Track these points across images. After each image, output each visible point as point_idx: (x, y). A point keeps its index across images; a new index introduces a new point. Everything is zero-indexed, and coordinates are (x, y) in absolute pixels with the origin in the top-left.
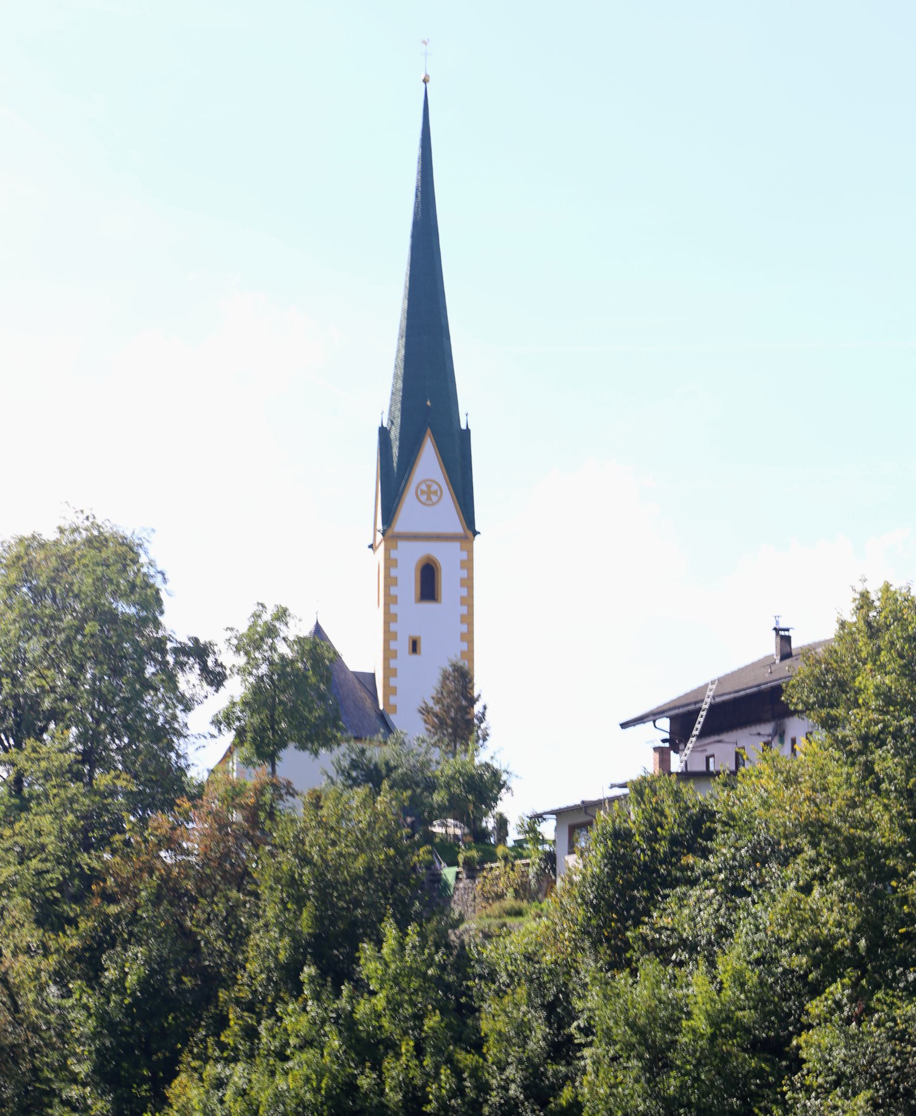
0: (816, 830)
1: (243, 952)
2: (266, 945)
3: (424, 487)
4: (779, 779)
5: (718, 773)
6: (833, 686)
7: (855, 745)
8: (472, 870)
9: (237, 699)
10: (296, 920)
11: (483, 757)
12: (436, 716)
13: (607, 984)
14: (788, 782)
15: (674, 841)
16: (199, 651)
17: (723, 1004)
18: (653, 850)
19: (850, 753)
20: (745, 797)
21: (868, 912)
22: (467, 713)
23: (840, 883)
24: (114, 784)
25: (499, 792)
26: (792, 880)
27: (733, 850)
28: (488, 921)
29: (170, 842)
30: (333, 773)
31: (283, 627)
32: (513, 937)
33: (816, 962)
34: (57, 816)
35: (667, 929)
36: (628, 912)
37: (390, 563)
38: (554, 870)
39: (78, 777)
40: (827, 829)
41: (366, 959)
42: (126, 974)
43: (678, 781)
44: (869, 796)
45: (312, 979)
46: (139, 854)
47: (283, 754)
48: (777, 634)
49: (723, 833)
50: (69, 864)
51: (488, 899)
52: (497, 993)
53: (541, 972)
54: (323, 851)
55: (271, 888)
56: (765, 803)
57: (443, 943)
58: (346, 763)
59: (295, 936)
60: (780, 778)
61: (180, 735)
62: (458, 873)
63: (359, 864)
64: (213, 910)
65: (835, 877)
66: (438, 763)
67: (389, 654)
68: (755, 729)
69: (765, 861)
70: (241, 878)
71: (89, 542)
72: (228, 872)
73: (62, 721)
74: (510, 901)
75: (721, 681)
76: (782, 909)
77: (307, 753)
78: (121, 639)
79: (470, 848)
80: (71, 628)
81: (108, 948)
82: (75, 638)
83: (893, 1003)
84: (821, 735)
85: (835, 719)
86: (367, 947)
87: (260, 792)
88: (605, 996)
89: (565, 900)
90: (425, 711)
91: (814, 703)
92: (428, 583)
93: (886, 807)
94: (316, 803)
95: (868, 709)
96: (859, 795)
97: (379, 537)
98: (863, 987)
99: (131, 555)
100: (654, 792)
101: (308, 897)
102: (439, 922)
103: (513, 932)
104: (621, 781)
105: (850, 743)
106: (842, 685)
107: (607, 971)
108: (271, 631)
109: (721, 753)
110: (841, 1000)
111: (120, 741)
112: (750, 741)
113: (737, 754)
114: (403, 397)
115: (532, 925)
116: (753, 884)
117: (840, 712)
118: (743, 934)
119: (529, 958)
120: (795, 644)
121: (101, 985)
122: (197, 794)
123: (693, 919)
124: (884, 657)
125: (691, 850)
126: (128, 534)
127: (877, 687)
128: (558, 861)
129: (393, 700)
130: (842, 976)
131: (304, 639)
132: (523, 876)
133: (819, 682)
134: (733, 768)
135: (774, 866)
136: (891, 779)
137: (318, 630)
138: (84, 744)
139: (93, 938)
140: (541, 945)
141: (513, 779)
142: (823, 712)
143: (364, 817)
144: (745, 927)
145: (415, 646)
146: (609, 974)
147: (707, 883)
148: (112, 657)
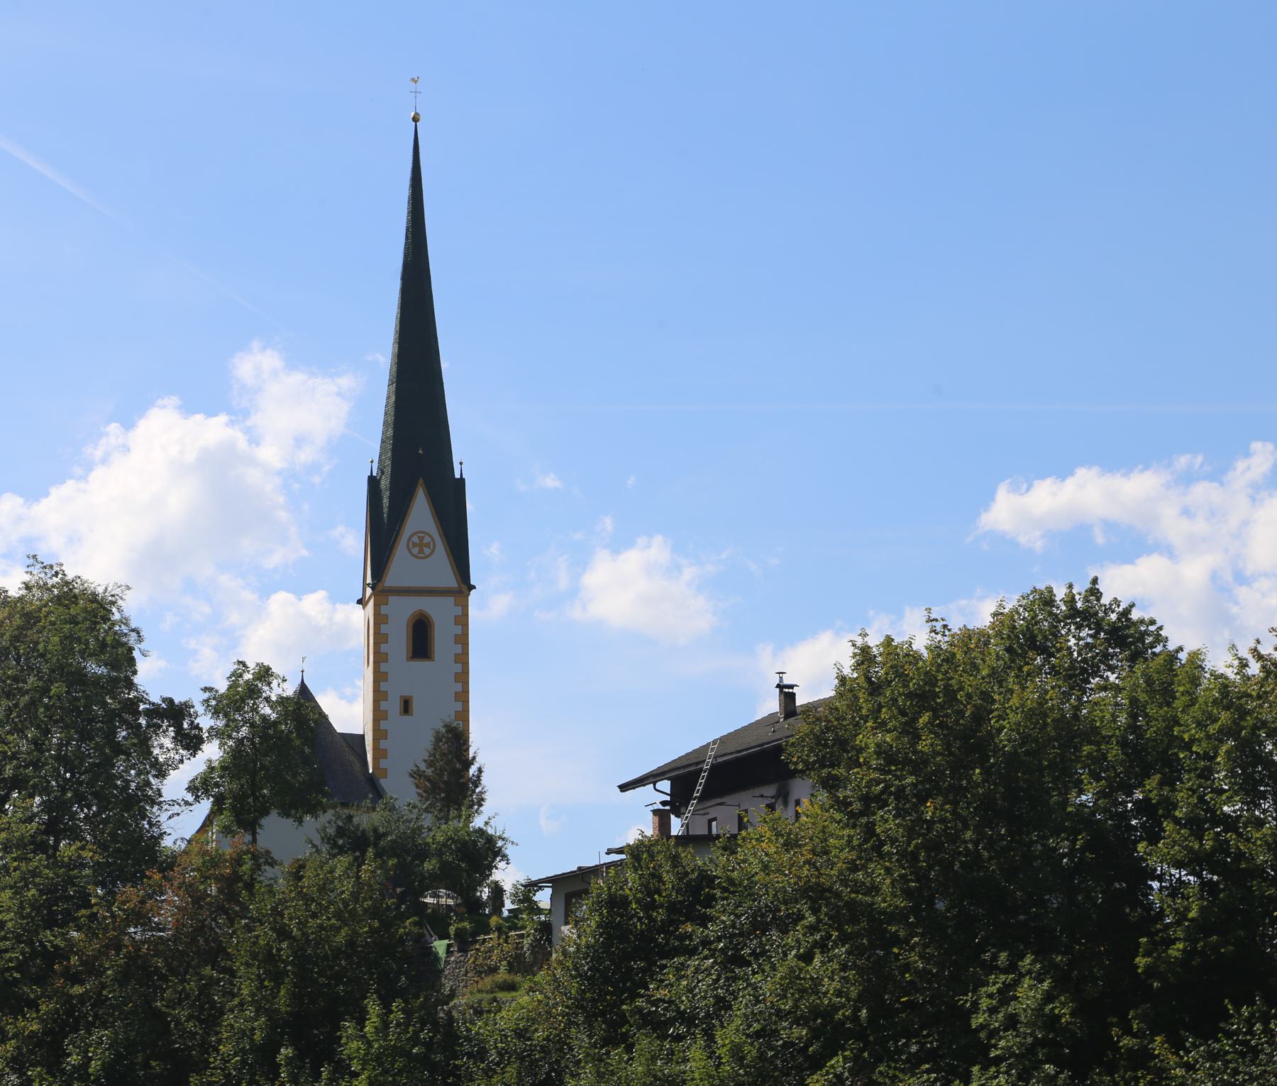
0: (815, 894)
1: (217, 1033)
2: (241, 1023)
3: (415, 539)
4: (773, 841)
5: (718, 837)
6: (833, 745)
7: (857, 806)
8: (464, 942)
9: (216, 764)
10: (274, 998)
11: (478, 822)
12: (429, 780)
13: (601, 1060)
14: (788, 845)
15: (672, 908)
16: (175, 713)
17: (722, 1081)
18: (650, 917)
19: (852, 815)
20: (744, 861)
21: (870, 980)
22: (462, 777)
23: (841, 951)
24: (79, 856)
25: (494, 860)
26: (793, 948)
27: (732, 917)
28: (479, 996)
29: (139, 917)
30: (317, 842)
31: (266, 688)
32: (504, 1013)
33: (815, 1034)
34: (17, 892)
35: (664, 1001)
36: (624, 984)
37: (380, 619)
38: (550, 941)
39: (41, 847)
40: (828, 894)
41: (348, 1038)
42: (91, 1059)
43: (677, 845)
44: (871, 860)
45: (289, 1061)
46: (106, 930)
47: (263, 821)
48: (781, 691)
49: (723, 899)
50: (30, 943)
51: (481, 973)
52: (486, 1072)
53: (532, 1049)
54: (302, 925)
55: (247, 965)
56: (765, 867)
57: (429, 1019)
58: (331, 831)
59: (271, 1014)
60: (781, 840)
61: (153, 803)
62: (449, 946)
63: (341, 938)
64: (184, 989)
65: (836, 945)
66: (430, 830)
67: (379, 715)
68: (757, 791)
69: (765, 929)
70: (216, 953)
71: (58, 600)
72: (200, 947)
73: (26, 789)
74: (502, 975)
75: (723, 740)
76: (782, 978)
77: (291, 820)
78: (89, 702)
79: (462, 920)
80: (35, 689)
81: (70, 1032)
82: (41, 701)
83: (895, 1076)
84: (823, 796)
85: (835, 778)
86: (349, 1026)
87: (238, 861)
88: (598, 1072)
89: (559, 973)
90: (416, 775)
91: (815, 762)
92: (421, 640)
93: (888, 870)
94: (297, 875)
95: (869, 768)
96: (861, 858)
97: (369, 591)
98: (864, 1059)
99: (102, 612)
100: (652, 857)
101: (286, 973)
102: (426, 999)
103: (504, 1008)
104: (618, 844)
105: (850, 804)
106: (843, 744)
107: (602, 1048)
108: (253, 691)
109: (723, 818)
110: (842, 1074)
111: (89, 809)
112: (754, 804)
113: (740, 818)
114: (393, 444)
115: (525, 999)
116: (753, 953)
117: (841, 771)
118: (742, 1006)
119: (521, 1034)
120: (800, 701)
121: (63, 1072)
122: (169, 864)
123: (691, 991)
124: (884, 714)
125: (690, 918)
126: (100, 590)
127: (878, 745)
128: (554, 932)
129: (383, 763)
130: (844, 1050)
131: (288, 698)
132: (517, 948)
133: (819, 741)
134: (736, 832)
135: (774, 934)
136: (894, 841)
137: (303, 690)
138: (49, 813)
139: (55, 1021)
140: (533, 1020)
141: (509, 846)
142: (824, 772)
143: (348, 886)
144: (744, 999)
145: (406, 706)
146: (603, 1051)
147: (706, 952)
148: (80, 720)
